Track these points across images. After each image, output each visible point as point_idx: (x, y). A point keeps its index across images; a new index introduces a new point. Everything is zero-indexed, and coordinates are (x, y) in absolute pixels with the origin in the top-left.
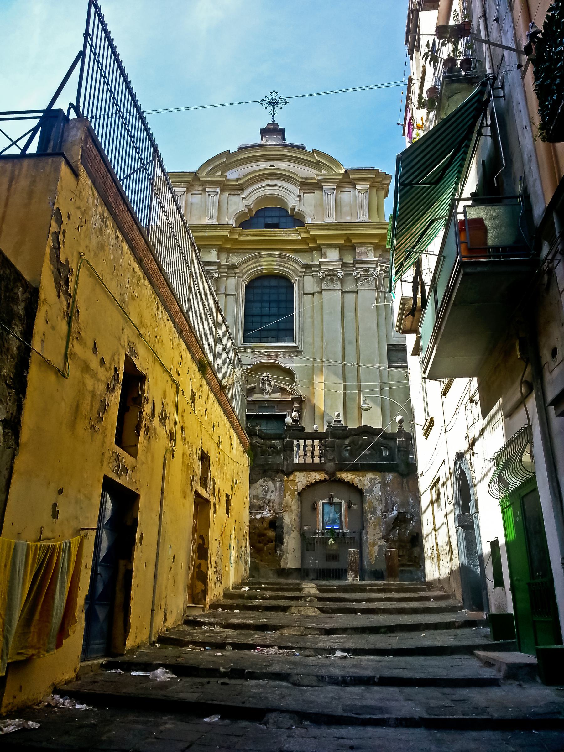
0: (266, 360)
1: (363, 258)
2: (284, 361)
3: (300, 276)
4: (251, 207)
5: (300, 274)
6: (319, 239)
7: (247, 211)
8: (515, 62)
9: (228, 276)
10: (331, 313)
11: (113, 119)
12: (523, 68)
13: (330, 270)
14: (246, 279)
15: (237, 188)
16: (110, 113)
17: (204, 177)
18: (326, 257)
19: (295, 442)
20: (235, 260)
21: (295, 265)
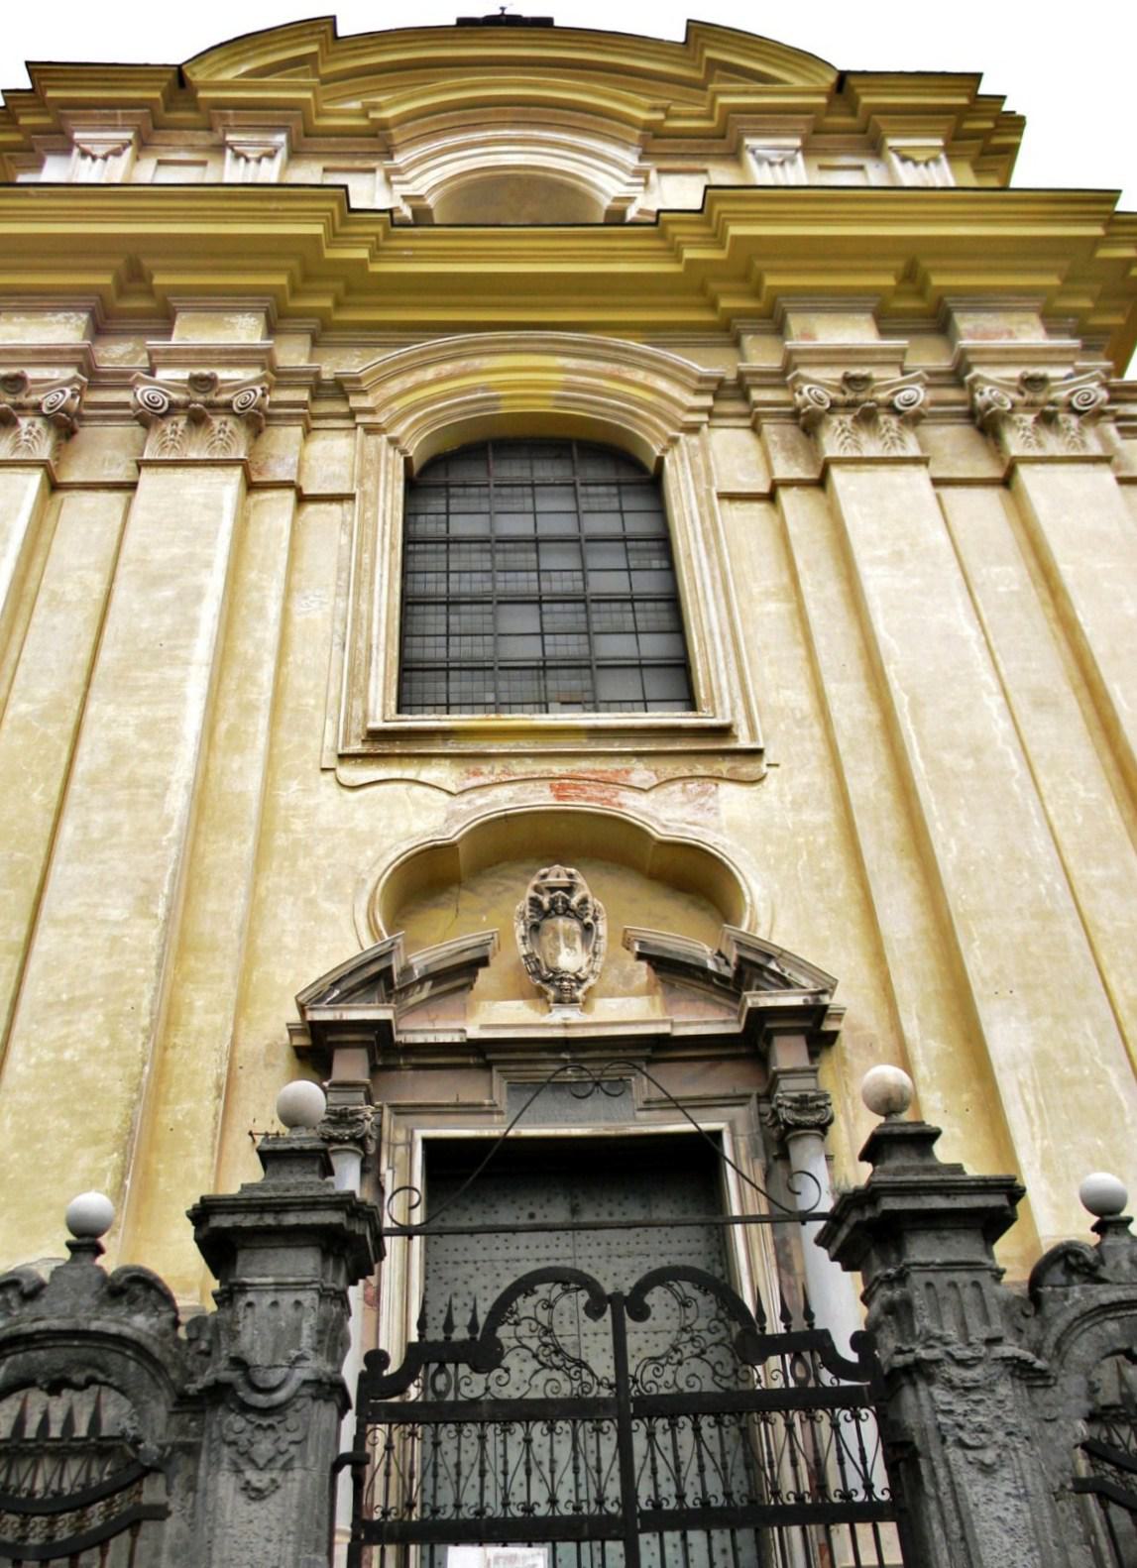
0: (542, 798)
2: (665, 807)
4: (430, 202)
13: (849, 381)
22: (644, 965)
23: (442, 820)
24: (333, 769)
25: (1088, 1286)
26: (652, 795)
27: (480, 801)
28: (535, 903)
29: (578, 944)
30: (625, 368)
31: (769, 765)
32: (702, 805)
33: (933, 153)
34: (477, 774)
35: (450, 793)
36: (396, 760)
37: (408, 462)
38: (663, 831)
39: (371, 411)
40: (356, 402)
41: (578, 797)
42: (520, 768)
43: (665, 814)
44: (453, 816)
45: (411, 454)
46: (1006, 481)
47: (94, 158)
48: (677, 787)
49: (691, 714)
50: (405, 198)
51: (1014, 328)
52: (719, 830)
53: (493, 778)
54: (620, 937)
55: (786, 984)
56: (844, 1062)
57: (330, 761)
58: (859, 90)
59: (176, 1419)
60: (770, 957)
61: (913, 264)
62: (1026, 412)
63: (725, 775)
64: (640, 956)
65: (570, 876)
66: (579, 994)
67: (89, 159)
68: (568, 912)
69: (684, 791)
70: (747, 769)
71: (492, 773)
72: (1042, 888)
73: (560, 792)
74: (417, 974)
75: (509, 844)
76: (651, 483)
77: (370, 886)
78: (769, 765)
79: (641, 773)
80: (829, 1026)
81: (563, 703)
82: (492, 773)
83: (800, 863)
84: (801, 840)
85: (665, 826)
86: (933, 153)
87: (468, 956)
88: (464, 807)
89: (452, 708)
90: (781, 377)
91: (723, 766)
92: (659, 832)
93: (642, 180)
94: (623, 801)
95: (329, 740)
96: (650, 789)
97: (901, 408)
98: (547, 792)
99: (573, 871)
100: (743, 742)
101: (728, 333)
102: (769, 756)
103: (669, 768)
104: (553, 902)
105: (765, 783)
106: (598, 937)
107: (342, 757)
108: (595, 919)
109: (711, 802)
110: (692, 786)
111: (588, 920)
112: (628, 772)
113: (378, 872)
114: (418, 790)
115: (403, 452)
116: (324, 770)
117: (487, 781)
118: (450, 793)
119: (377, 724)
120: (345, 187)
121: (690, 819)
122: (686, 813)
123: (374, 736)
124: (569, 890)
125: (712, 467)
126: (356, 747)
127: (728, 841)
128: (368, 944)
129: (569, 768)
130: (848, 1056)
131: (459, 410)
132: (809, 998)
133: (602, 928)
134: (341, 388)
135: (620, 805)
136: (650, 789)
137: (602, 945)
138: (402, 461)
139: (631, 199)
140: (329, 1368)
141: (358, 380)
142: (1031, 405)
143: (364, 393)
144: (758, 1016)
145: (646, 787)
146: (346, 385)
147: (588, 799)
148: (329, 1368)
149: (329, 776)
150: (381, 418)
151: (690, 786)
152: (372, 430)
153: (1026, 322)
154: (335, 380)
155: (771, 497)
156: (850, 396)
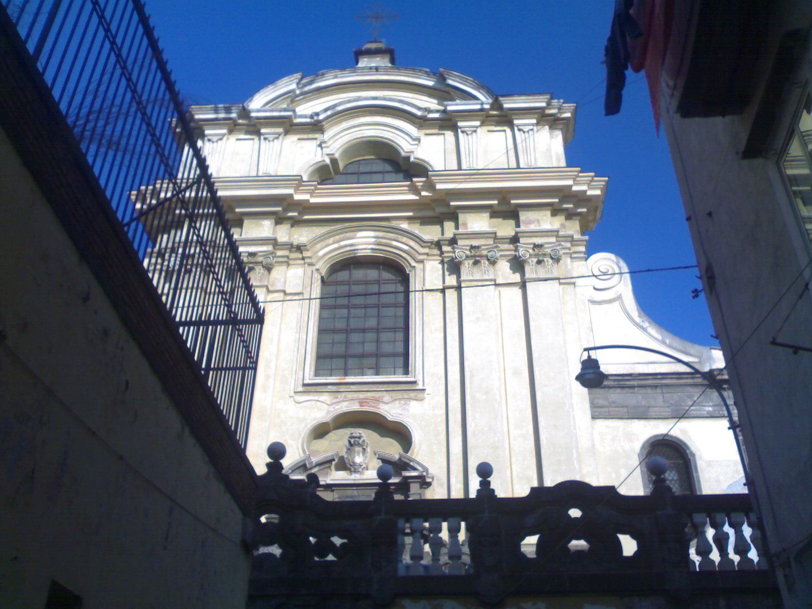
0: (356, 407)
1: (532, 227)
2: (391, 410)
3: (422, 261)
4: (337, 156)
5: (421, 257)
6: (516, 119)
7: (328, 161)
8: (558, 160)
9: (291, 262)
10: (478, 319)
11: (124, 169)
12: (478, 259)
13: (472, 247)
14: (323, 267)
15: (315, 127)
16: (124, 169)
17: (258, 111)
18: (467, 228)
19: (753, 555)
20: (302, 235)
21: (412, 243)
22: (380, 461)
23: (325, 414)
24: (293, 397)
25: (467, 543)
26: (389, 405)
27: (337, 407)
28: (350, 442)
29: (361, 455)
30: (399, 236)
31: (427, 394)
32: (404, 408)
33: (531, 127)
34: (337, 398)
35: (328, 405)
36: (312, 393)
37: (322, 277)
38: (391, 417)
39: (310, 257)
40: (306, 254)
41: (367, 406)
42: (350, 396)
43: (393, 412)
44: (328, 412)
45: (323, 275)
46: (523, 285)
47: (213, 142)
48: (397, 402)
49: (405, 376)
50: (328, 155)
51: (540, 218)
52: (408, 417)
53: (341, 399)
54: (373, 452)
55: (415, 469)
56: (434, 490)
57: (292, 394)
58: (502, 102)
59: (554, 137)
60: (411, 461)
61: (503, 195)
62: (534, 258)
63: (413, 398)
64: (378, 459)
65: (360, 434)
66: (360, 470)
67: (211, 142)
68: (359, 445)
69: (399, 403)
70: (420, 395)
71: (341, 398)
72: (496, 438)
73: (361, 403)
74: (314, 464)
75: (346, 421)
76: (404, 279)
77: (303, 435)
78: (427, 394)
79: (387, 397)
80: (428, 480)
81: (369, 368)
82: (341, 398)
83: (432, 428)
84: (433, 420)
85: (392, 416)
86: (531, 127)
87: (329, 458)
88: (332, 409)
89: (333, 372)
90: (453, 242)
91: (412, 395)
92: (390, 418)
93: (417, 142)
94: (379, 407)
95: (292, 388)
96: (389, 402)
97: (490, 259)
98: (358, 404)
99: (360, 432)
100: (420, 387)
101: (438, 220)
102: (427, 392)
103: (394, 394)
104: (355, 441)
105: (425, 400)
106: (367, 452)
107: (295, 392)
108: (367, 447)
109: (407, 407)
110: (402, 402)
111: (365, 447)
112: (383, 397)
113: (305, 431)
114: (319, 403)
115: (320, 274)
116: (291, 397)
117: (339, 400)
118: (328, 405)
119: (307, 381)
120: (310, 380)
121: (400, 413)
122: (399, 411)
123: (304, 385)
124: (360, 438)
125: (428, 274)
126: (301, 389)
127: (410, 420)
128: (302, 455)
129: (365, 395)
130: (435, 488)
131: (340, 255)
132: (420, 473)
133: (369, 449)
134: (299, 248)
135: (379, 408)
136: (389, 402)
137: (368, 455)
138: (320, 277)
139: (412, 152)
140: (332, 428)
141: (306, 246)
142: (536, 255)
143: (308, 250)
144: (407, 478)
145: (388, 402)
146: (302, 248)
147: (370, 406)
148: (332, 428)
149: (292, 399)
150: (314, 261)
151: (401, 402)
152: (311, 264)
153: (545, 216)
154: (297, 245)
155: (443, 291)
156: (473, 253)
